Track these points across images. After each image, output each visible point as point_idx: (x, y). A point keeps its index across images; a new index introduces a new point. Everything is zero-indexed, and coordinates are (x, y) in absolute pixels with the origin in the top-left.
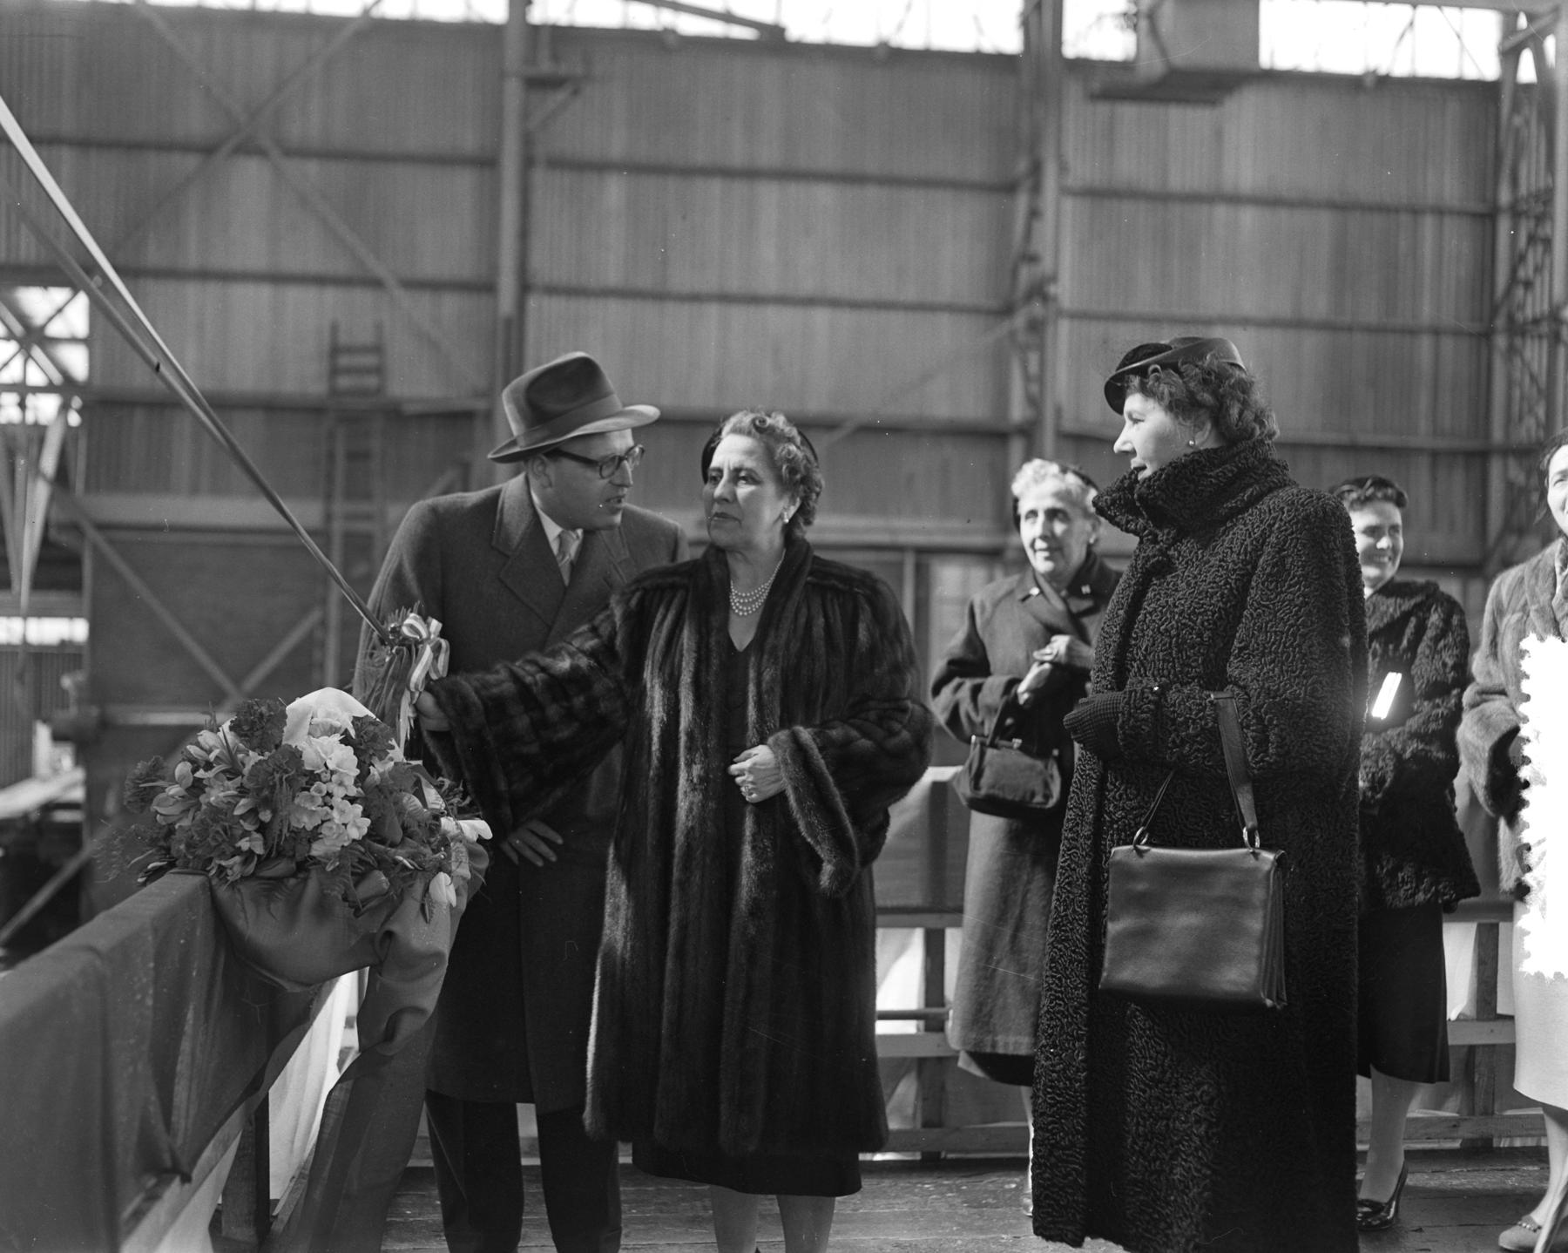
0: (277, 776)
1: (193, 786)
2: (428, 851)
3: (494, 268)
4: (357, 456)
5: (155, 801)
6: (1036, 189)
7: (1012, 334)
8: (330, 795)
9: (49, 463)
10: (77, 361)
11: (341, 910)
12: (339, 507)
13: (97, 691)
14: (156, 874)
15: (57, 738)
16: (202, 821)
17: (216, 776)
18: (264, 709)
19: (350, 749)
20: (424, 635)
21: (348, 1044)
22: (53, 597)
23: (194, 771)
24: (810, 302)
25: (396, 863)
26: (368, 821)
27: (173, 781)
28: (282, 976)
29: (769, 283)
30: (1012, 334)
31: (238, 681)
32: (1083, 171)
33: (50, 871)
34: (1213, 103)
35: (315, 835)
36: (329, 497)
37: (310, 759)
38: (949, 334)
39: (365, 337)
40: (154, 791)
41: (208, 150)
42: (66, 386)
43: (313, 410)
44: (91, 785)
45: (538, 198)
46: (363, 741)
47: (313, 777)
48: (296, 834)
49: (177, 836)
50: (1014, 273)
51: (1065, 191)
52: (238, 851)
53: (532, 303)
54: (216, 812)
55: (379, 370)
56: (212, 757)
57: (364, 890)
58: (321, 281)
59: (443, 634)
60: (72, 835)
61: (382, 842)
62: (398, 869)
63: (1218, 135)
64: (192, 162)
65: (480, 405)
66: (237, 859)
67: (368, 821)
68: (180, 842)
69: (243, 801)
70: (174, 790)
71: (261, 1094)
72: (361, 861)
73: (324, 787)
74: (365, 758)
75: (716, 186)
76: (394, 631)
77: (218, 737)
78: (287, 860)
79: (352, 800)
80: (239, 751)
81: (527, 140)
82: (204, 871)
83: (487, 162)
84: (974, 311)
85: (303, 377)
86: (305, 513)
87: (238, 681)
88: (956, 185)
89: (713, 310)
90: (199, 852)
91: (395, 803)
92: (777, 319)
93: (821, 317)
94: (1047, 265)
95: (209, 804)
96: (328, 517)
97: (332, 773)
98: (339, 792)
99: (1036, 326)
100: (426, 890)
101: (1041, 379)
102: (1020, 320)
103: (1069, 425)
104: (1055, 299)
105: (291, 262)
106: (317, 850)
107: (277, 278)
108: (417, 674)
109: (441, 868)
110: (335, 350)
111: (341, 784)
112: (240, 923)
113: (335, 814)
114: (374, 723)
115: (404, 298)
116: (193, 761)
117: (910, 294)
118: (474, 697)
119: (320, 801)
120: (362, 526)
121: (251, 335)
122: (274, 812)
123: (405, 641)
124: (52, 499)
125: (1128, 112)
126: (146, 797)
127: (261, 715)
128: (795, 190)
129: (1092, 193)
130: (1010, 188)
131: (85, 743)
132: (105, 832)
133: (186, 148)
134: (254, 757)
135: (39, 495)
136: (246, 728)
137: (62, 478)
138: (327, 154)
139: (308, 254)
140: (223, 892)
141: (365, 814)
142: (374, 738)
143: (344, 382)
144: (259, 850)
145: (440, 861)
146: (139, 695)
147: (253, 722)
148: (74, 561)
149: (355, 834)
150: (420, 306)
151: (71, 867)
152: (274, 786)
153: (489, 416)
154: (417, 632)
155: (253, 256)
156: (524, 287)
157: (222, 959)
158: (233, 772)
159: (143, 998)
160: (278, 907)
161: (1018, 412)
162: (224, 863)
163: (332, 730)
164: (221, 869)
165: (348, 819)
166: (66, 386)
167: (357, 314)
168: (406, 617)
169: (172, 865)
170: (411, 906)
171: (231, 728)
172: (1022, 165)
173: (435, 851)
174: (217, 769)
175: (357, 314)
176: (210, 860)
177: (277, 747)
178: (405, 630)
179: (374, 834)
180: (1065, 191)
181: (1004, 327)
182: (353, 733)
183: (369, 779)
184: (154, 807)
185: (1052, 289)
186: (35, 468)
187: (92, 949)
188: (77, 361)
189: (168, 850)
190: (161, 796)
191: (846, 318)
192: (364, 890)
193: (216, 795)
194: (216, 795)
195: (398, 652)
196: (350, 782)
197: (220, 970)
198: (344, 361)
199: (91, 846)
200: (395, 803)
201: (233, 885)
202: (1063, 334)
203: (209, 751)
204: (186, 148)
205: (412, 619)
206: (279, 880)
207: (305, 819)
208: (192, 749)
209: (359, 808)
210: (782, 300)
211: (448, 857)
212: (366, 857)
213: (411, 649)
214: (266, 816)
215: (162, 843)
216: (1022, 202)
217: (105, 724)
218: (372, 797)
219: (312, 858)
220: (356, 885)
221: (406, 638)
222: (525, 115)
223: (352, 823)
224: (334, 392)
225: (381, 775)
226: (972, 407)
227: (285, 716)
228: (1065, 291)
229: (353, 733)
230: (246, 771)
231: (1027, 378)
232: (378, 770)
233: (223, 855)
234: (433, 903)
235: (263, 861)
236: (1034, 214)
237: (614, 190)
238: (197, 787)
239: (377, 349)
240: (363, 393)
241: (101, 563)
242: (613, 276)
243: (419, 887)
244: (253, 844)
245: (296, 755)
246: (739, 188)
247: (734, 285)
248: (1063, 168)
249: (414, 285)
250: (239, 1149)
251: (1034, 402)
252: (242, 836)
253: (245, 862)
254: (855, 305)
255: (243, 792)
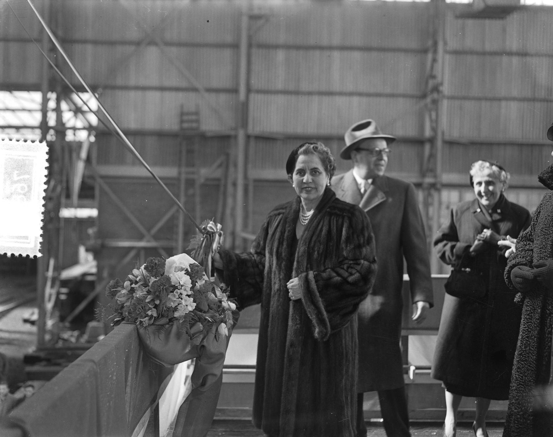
0: (162, 287)
1: (131, 290)
2: (217, 315)
3: (238, 84)
4: (190, 152)
5: (117, 296)
6: (435, 52)
7: (426, 105)
8: (181, 294)
9: (84, 154)
10: (93, 120)
11: (185, 336)
12: (184, 169)
13: (101, 234)
14: (117, 323)
15: (87, 250)
16: (134, 304)
17: (139, 287)
18: (157, 261)
19: (188, 277)
20: (215, 231)
21: (188, 374)
22: (86, 202)
23: (131, 284)
24: (351, 94)
25: (206, 319)
26: (195, 304)
27: (123, 288)
28: (163, 361)
29: (336, 87)
30: (426, 105)
31: (149, 230)
32: (453, 44)
33: (84, 297)
34: (502, 18)
35: (176, 309)
36: (180, 166)
37: (173, 280)
38: (402, 104)
39: (193, 109)
40: (117, 292)
41: (138, 44)
42: (90, 128)
43: (173, 135)
44: (99, 267)
45: (254, 59)
46: (193, 273)
47: (175, 288)
48: (169, 309)
49: (125, 309)
50: (427, 83)
51: (446, 52)
52: (147, 315)
53: (252, 96)
54: (140, 301)
55: (197, 121)
56: (138, 279)
57: (193, 331)
58: (177, 89)
59: (222, 229)
60: (92, 284)
61: (201, 311)
62: (206, 322)
63: (504, 30)
64: (132, 48)
65: (233, 133)
66: (147, 318)
67: (195, 304)
68: (126, 311)
69: (149, 296)
70: (124, 292)
71: (156, 403)
72: (192, 319)
73: (179, 291)
74: (194, 279)
75: (317, 53)
76: (204, 228)
77: (140, 272)
78: (165, 317)
79: (189, 296)
80: (147, 276)
81: (250, 38)
82: (135, 322)
83: (235, 46)
84: (412, 97)
85: (171, 124)
86: (171, 172)
87: (149, 230)
88: (406, 51)
89: (316, 98)
90: (133, 315)
91: (206, 297)
92: (340, 101)
93: (355, 100)
94: (439, 79)
95: (136, 298)
96: (180, 173)
97: (182, 286)
98: (185, 293)
99: (435, 102)
100: (217, 329)
101: (437, 121)
102: (429, 100)
103: (447, 138)
104: (442, 92)
105: (167, 83)
106: (176, 315)
107: (162, 89)
108: (215, 246)
109: (222, 321)
110: (182, 114)
111: (185, 290)
112: (148, 342)
113: (183, 301)
114: (197, 266)
115: (206, 95)
116: (130, 280)
117: (388, 90)
118: (235, 258)
119: (177, 297)
120: (191, 176)
121: (152, 110)
122: (161, 301)
123: (208, 233)
124: (86, 168)
125: (470, 22)
126: (113, 294)
127: (156, 263)
128: (346, 54)
129: (456, 53)
130: (425, 51)
131: (98, 253)
132: (103, 283)
133: (130, 43)
134: (153, 279)
135: (80, 167)
136: (150, 268)
137: (88, 160)
138: (180, 44)
139: (174, 81)
140: (142, 331)
141: (194, 301)
142: (197, 272)
143: (185, 125)
144: (155, 315)
145: (222, 318)
146: (116, 236)
147: (153, 267)
148: (92, 188)
149: (190, 309)
150: (212, 98)
151: (91, 296)
152: (160, 291)
153: (236, 137)
154: (213, 229)
155: (154, 81)
156: (249, 90)
157: (142, 354)
158: (145, 285)
159: (112, 377)
160: (162, 336)
161: (428, 133)
162: (142, 320)
163: (182, 269)
164: (141, 322)
165: (188, 303)
166: (90, 128)
167: (190, 101)
168: (208, 223)
169: (123, 319)
170: (211, 336)
171: (145, 268)
172: (430, 43)
173: (220, 315)
174: (139, 284)
175: (190, 101)
176: (137, 318)
177: (162, 275)
178: (208, 228)
179: (197, 308)
180: (446, 52)
181: (422, 103)
182: (189, 270)
183: (195, 288)
184: (116, 298)
185: (441, 88)
186: (79, 157)
187: (93, 361)
188: (93, 120)
189: (122, 314)
190: (119, 294)
191: (364, 100)
192: (193, 331)
193: (139, 294)
194: (139, 294)
195: (206, 237)
196: (188, 289)
197: (141, 359)
198: (185, 118)
199: (99, 288)
200: (206, 297)
201: (145, 327)
202: (445, 105)
203: (137, 277)
204: (130, 43)
205: (211, 224)
206: (163, 325)
207: (172, 304)
208: (130, 276)
209: (192, 299)
210: (341, 94)
211: (225, 317)
212: (195, 317)
213: (210, 236)
214: (157, 302)
215: (119, 311)
216: (430, 56)
217: (103, 246)
218: (197, 295)
219: (175, 317)
220: (190, 328)
221: (209, 231)
222: (249, 29)
223: (189, 305)
224: (182, 129)
225: (200, 286)
226: (411, 132)
227: (165, 264)
228: (446, 89)
229: (189, 270)
230: (150, 284)
231: (431, 121)
232: (199, 284)
233: (142, 317)
234: (219, 334)
235: (156, 319)
236: (434, 60)
237: (281, 55)
238: (132, 290)
239: (197, 113)
240: (192, 129)
241: (102, 190)
242: (280, 86)
243: (214, 328)
244: (153, 312)
245: (168, 279)
246: (326, 53)
247: (324, 88)
248: (445, 43)
249: (209, 90)
250: (148, 425)
251: (434, 130)
252: (149, 310)
253: (150, 319)
254: (368, 95)
255: (149, 292)
